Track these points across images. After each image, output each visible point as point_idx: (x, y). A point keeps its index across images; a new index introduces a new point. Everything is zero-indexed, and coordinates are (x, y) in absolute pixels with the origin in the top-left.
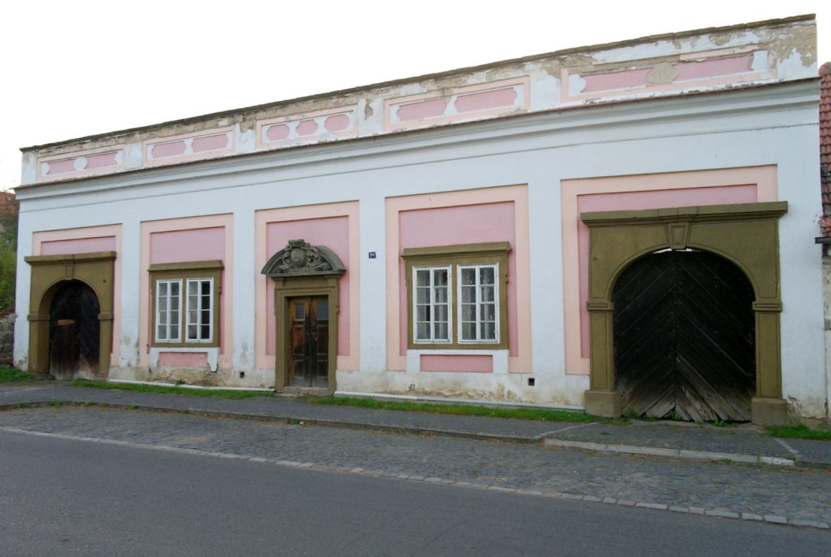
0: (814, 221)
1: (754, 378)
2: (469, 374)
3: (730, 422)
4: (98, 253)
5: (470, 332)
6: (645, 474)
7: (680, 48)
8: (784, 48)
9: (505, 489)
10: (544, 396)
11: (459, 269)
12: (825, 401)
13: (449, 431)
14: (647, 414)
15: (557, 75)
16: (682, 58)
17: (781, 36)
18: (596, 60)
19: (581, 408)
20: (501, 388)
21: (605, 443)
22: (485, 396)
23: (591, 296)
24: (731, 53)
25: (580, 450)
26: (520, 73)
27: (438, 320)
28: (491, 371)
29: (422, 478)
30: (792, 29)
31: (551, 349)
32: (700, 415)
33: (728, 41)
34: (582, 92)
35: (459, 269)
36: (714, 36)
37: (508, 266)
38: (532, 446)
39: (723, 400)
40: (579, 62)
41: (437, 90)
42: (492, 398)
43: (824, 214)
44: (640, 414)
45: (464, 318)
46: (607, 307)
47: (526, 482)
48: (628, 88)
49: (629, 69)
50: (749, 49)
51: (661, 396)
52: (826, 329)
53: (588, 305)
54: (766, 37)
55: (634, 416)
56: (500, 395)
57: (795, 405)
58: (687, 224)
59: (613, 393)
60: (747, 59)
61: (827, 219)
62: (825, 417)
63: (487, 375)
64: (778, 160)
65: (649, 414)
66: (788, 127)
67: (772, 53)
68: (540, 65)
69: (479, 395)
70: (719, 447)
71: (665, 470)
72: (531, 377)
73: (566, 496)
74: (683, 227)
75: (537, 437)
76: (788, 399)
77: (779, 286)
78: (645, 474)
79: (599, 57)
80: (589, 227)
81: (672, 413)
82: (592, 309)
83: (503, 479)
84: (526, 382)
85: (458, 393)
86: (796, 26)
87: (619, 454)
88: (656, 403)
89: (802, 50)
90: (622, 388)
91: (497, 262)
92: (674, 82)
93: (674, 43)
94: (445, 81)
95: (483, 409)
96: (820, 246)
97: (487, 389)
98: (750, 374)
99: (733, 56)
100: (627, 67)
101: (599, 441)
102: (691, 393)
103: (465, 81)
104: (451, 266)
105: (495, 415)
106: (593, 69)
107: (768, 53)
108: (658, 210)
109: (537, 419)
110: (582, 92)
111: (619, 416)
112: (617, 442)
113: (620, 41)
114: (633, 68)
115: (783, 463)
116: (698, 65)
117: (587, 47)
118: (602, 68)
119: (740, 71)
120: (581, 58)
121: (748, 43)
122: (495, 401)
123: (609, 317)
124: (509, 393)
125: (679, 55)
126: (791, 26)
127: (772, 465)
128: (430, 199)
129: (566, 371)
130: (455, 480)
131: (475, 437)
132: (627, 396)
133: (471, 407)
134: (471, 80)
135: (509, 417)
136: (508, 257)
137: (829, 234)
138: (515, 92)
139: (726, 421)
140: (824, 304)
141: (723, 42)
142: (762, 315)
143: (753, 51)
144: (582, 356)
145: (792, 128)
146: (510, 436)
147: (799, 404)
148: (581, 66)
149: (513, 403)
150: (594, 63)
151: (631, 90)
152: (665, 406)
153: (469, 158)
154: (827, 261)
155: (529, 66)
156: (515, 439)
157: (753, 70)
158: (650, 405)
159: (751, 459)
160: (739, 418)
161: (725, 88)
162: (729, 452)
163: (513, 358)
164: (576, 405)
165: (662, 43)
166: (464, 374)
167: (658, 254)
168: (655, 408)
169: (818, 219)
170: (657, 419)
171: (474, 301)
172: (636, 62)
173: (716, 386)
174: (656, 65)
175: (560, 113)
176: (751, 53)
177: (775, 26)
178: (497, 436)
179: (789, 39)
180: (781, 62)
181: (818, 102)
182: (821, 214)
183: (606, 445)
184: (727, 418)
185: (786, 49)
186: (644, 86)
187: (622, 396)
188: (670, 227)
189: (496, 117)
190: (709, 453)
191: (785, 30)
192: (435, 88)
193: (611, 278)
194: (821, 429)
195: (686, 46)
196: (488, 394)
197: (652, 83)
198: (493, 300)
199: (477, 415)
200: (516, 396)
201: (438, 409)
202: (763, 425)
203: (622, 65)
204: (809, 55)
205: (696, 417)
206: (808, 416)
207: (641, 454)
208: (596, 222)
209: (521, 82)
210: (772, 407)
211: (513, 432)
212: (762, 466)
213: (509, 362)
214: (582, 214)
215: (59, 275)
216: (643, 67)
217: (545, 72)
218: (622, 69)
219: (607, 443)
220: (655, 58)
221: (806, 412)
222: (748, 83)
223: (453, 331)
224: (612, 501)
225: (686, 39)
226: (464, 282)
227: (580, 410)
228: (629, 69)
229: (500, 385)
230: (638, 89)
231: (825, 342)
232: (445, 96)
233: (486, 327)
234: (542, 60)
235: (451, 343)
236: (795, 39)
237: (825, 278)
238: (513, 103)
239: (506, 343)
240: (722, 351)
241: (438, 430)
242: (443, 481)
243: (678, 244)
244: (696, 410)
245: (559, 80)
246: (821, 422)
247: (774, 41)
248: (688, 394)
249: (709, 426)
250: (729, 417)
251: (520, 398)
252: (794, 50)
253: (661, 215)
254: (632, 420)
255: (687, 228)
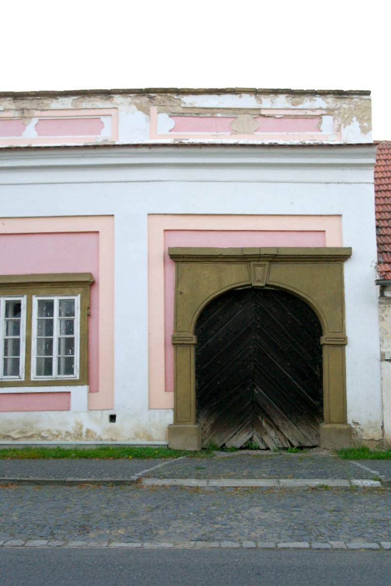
0: (371, 266)
1: (322, 405)
2: (43, 413)
3: (301, 448)
4: (308, 248)
5: (46, 368)
6: (261, 508)
7: (261, 103)
8: (346, 116)
9: (130, 545)
10: (126, 433)
11: (35, 300)
12: (382, 424)
13: (31, 478)
14: (226, 445)
15: (147, 112)
16: (263, 112)
17: (344, 106)
18: (185, 103)
19: (165, 443)
20: (79, 427)
21: (205, 478)
22: (60, 436)
23: (176, 329)
24: (304, 114)
25: (182, 488)
26: (107, 104)
27: (46, 359)
28: (68, 409)
29: (21, 542)
30: (352, 101)
31: (134, 382)
32: (275, 443)
33: (301, 103)
34: (170, 131)
35: (35, 300)
36: (290, 97)
37: (90, 298)
38: (131, 487)
39: (295, 427)
40: (168, 102)
41: (16, 110)
42: (68, 438)
43: (378, 261)
44: (220, 444)
45: (39, 353)
46: (192, 340)
47: (147, 533)
48: (215, 133)
49: (215, 115)
50: (318, 113)
51: (237, 429)
52: (382, 361)
53: (173, 338)
54: (333, 104)
55: (215, 448)
56: (78, 435)
57: (357, 429)
58: (267, 263)
59: (197, 426)
60: (317, 121)
61: (381, 265)
62: (382, 438)
63: (64, 413)
64: (342, 211)
65: (228, 445)
66: (351, 183)
67: (337, 119)
68: (129, 99)
69: (54, 435)
70: (311, 473)
71: (256, 501)
72: (112, 413)
73: (200, 544)
74: (264, 266)
75: (134, 478)
76: (352, 424)
77: (344, 322)
78: (261, 508)
79: (188, 100)
80: (176, 261)
81: (249, 442)
82: (177, 343)
83: (120, 531)
84: (107, 418)
85: (29, 434)
86: (356, 99)
87: (223, 489)
88: (235, 434)
89: (360, 120)
90: (202, 420)
91: (78, 294)
92: (255, 133)
93: (256, 97)
94: (25, 101)
95: (60, 451)
96: (378, 286)
97: (63, 429)
98: (317, 403)
99: (305, 117)
100: (213, 114)
101: (198, 477)
102: (266, 422)
103: (48, 105)
104: (26, 296)
105: (75, 457)
106: (182, 111)
107: (334, 119)
108: (242, 249)
109: (123, 457)
110: (170, 131)
111: (200, 449)
112: (217, 477)
113: (208, 88)
114: (219, 115)
115: (372, 485)
116: (277, 120)
117: (177, 89)
118: (188, 111)
119: (311, 131)
120: (170, 99)
121: (318, 107)
122: (71, 441)
123: (193, 349)
124: (88, 431)
125: (259, 109)
126: (352, 99)
127: (364, 487)
128: (3, 224)
129: (149, 405)
130: (64, 539)
131: (63, 483)
132: (208, 428)
133: (46, 449)
134: (55, 104)
135: (93, 457)
136: (91, 288)
137: (386, 277)
138: (102, 122)
139: (298, 447)
140: (380, 338)
141: (298, 103)
142: (331, 348)
143: (322, 115)
144: (166, 390)
145: (353, 185)
146: (105, 479)
147: (361, 428)
148: (170, 106)
149: (92, 442)
150: (183, 105)
151: (217, 136)
152: (243, 437)
153: (126, 182)
154: (382, 301)
155: (118, 99)
156: (111, 481)
157: (321, 131)
158: (230, 436)
159: (344, 483)
160: (308, 444)
161: (300, 144)
162: (322, 478)
163: (91, 394)
164: (159, 440)
165: (245, 96)
166: (37, 413)
167: (238, 290)
168: (234, 438)
169: (374, 265)
170: (236, 449)
171: (51, 334)
172: (222, 110)
173: (289, 415)
174: (239, 116)
175: (150, 148)
176: (320, 117)
177: (340, 96)
178: (89, 480)
179: (350, 109)
180: (344, 127)
181: (373, 164)
182: (376, 260)
183: (207, 480)
184: (299, 445)
185: (348, 117)
186: (229, 133)
187: (202, 429)
188: (252, 265)
189: (81, 144)
190: (306, 480)
191: (347, 101)
192: (13, 107)
193: (196, 311)
194: (380, 450)
195: (266, 102)
196: (64, 434)
197: (236, 131)
198: (72, 333)
199: (55, 457)
200: (95, 434)
201: (9, 454)
202: (332, 449)
203: (208, 110)
204: (366, 124)
205: (271, 446)
206: (368, 439)
207: (244, 487)
208: (184, 258)
209: (109, 113)
210: (340, 432)
211: (107, 474)
212: (356, 489)
213: (89, 399)
214: (169, 248)
215: (234, 277)
216: (228, 116)
217: (134, 107)
218: (209, 115)
219: (207, 477)
220: (239, 109)
221: (366, 435)
222: (319, 142)
223: (26, 367)
224: (251, 544)
225: (266, 96)
226: (40, 313)
227: (164, 445)
228: (215, 115)
229: (77, 423)
230: (223, 135)
231: (381, 372)
232: (25, 117)
233: (10, 363)
234: (131, 95)
235: (23, 379)
236: (355, 109)
237: (380, 316)
238: (100, 134)
239: (86, 378)
240: (294, 382)
241: (18, 479)
242: (50, 544)
243: (259, 281)
244: (271, 438)
245: (148, 117)
246: (378, 443)
247: (338, 109)
248: (264, 424)
249: (284, 453)
250: (300, 443)
251: (100, 436)
252: (354, 119)
253: (245, 253)
254: (215, 452)
255: (267, 266)
